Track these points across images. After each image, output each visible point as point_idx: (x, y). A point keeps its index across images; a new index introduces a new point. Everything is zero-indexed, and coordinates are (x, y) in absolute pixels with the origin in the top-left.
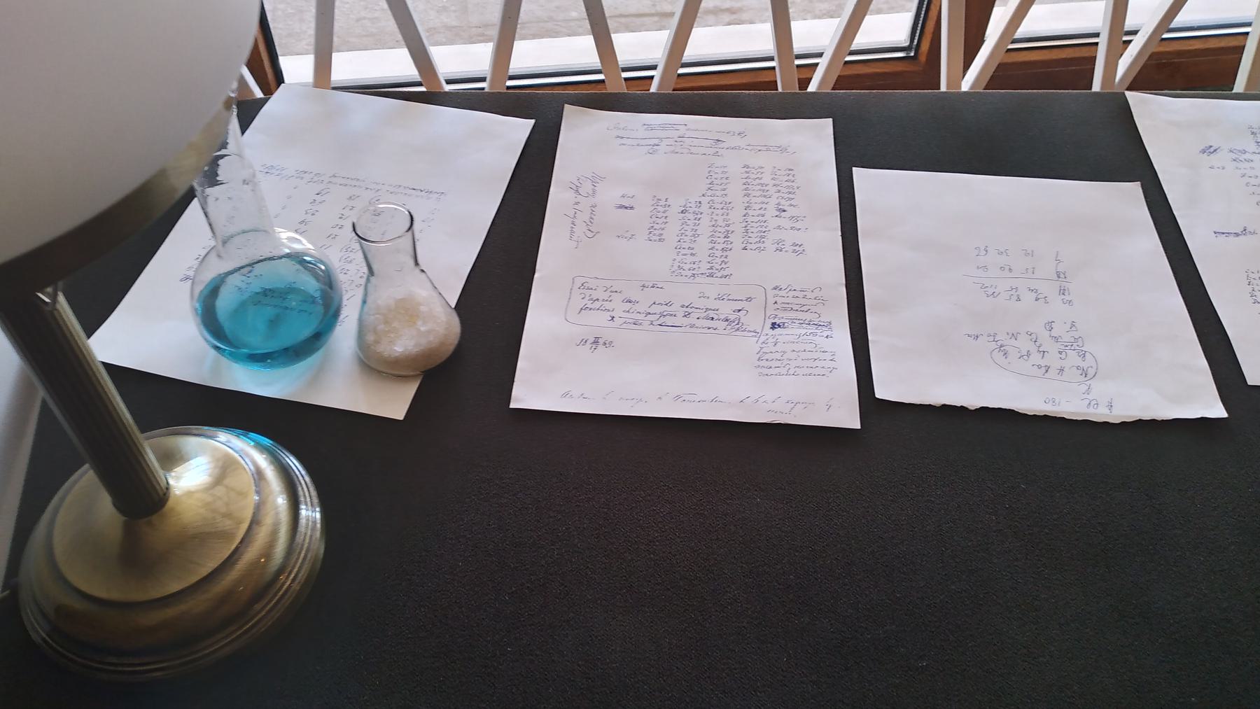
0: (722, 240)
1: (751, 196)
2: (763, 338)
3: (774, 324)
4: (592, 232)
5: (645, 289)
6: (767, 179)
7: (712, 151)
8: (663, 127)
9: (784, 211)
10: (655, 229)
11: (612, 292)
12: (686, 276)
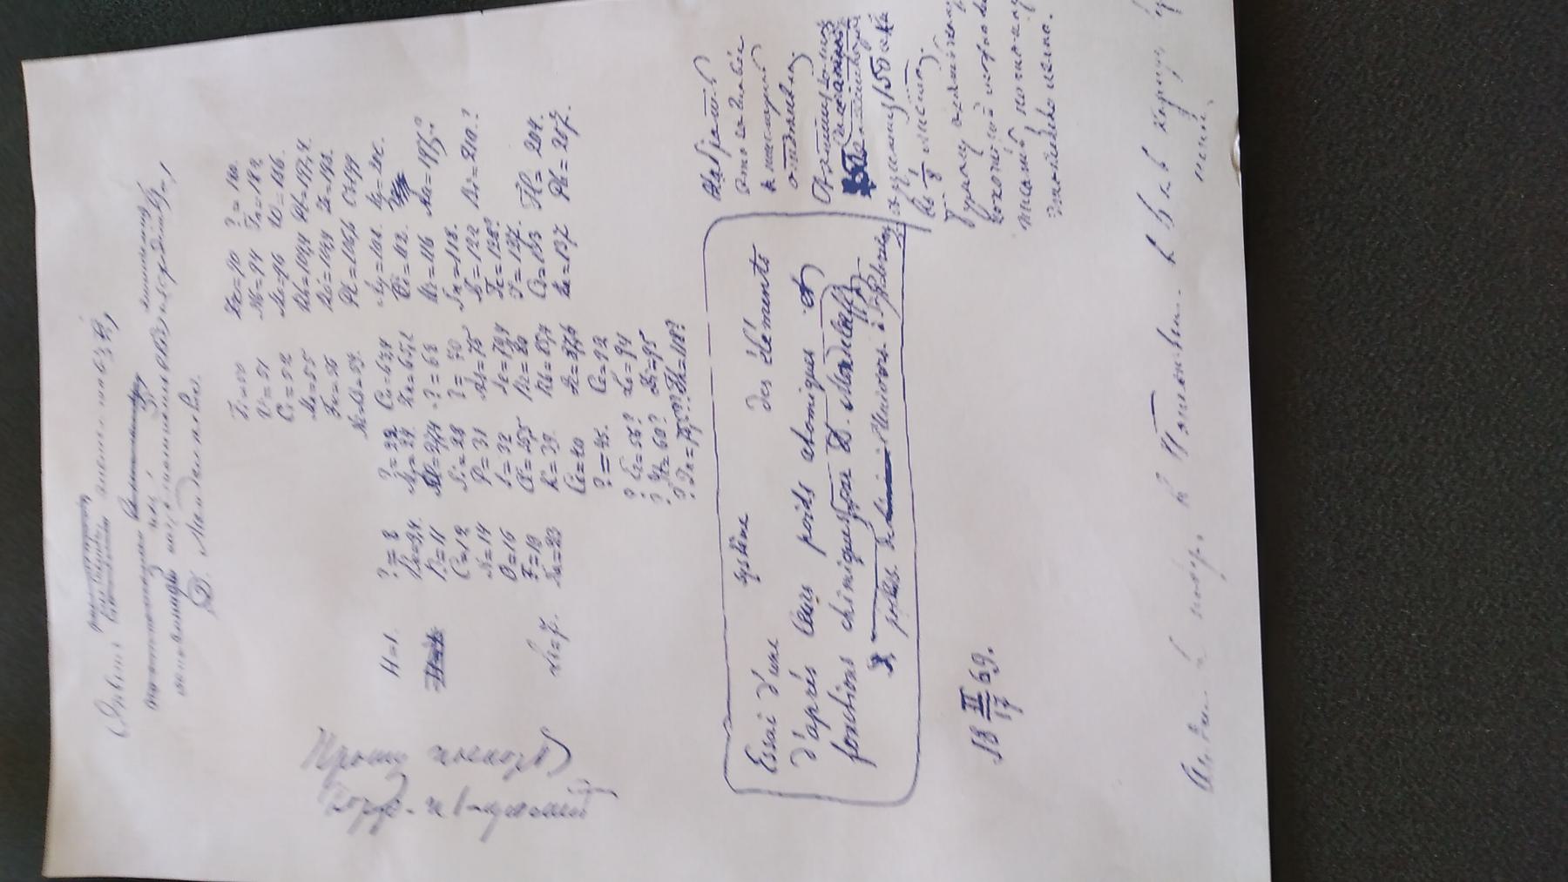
0: (536, 360)
1: (350, 283)
2: (909, 214)
3: (849, 187)
4: (545, 750)
5: (753, 571)
6: (282, 241)
7: (181, 415)
8: (98, 567)
9: (402, 181)
10: (513, 560)
11: (775, 670)
12: (690, 454)
